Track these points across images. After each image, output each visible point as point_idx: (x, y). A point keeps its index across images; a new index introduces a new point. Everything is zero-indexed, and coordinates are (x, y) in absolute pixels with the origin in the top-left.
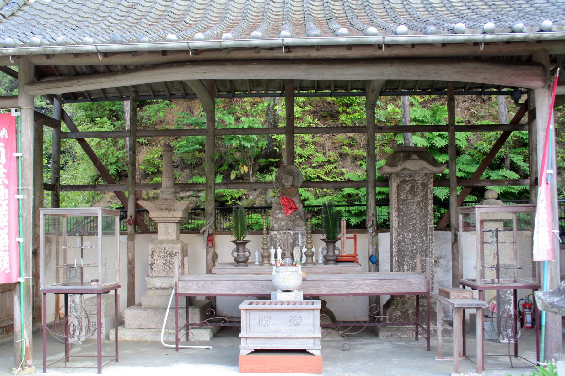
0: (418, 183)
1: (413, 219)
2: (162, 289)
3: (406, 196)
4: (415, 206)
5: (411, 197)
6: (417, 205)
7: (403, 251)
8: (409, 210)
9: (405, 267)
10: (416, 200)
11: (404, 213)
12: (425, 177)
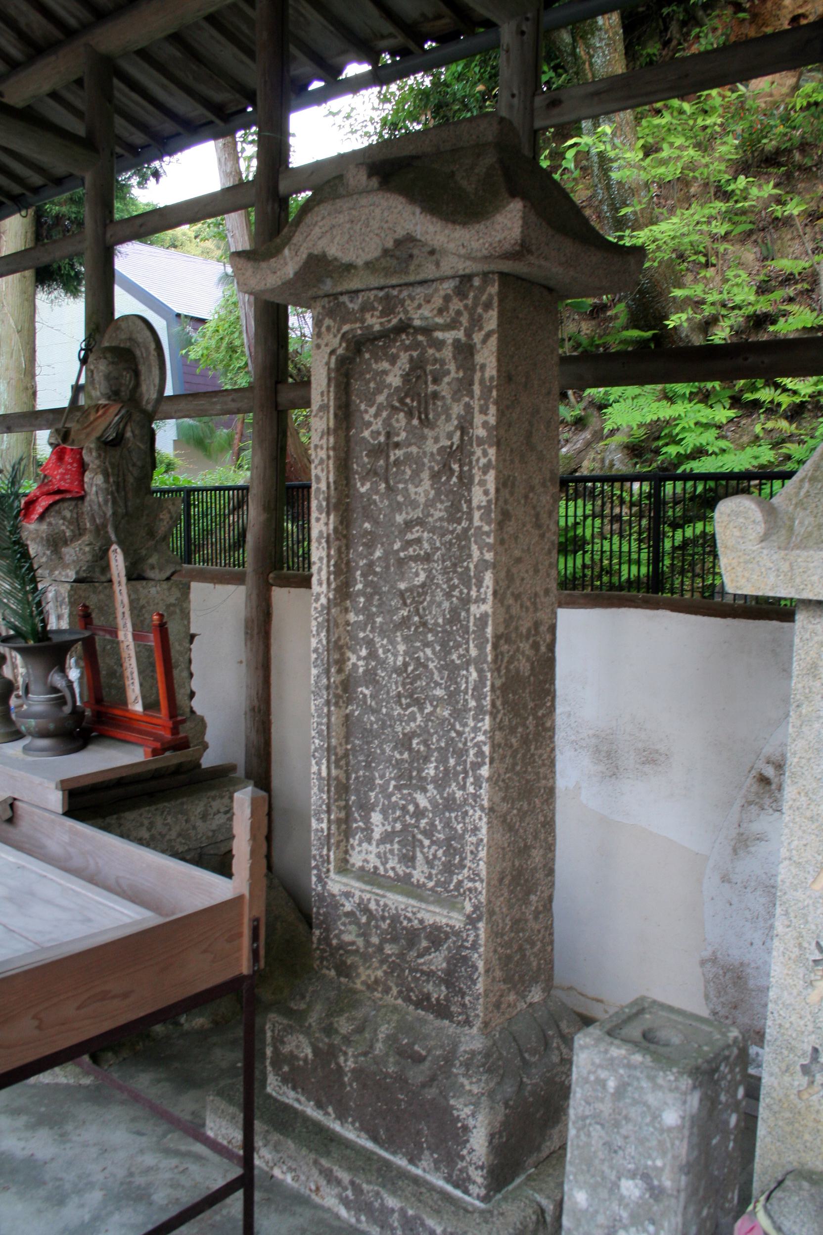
0: (439, 345)
1: (416, 558)
2: (269, 814)
3: (387, 422)
4: (427, 484)
5: (409, 429)
6: (435, 476)
7: (368, 734)
8: (399, 507)
9: (376, 817)
10: (431, 447)
11: (376, 522)
12: (456, 305)
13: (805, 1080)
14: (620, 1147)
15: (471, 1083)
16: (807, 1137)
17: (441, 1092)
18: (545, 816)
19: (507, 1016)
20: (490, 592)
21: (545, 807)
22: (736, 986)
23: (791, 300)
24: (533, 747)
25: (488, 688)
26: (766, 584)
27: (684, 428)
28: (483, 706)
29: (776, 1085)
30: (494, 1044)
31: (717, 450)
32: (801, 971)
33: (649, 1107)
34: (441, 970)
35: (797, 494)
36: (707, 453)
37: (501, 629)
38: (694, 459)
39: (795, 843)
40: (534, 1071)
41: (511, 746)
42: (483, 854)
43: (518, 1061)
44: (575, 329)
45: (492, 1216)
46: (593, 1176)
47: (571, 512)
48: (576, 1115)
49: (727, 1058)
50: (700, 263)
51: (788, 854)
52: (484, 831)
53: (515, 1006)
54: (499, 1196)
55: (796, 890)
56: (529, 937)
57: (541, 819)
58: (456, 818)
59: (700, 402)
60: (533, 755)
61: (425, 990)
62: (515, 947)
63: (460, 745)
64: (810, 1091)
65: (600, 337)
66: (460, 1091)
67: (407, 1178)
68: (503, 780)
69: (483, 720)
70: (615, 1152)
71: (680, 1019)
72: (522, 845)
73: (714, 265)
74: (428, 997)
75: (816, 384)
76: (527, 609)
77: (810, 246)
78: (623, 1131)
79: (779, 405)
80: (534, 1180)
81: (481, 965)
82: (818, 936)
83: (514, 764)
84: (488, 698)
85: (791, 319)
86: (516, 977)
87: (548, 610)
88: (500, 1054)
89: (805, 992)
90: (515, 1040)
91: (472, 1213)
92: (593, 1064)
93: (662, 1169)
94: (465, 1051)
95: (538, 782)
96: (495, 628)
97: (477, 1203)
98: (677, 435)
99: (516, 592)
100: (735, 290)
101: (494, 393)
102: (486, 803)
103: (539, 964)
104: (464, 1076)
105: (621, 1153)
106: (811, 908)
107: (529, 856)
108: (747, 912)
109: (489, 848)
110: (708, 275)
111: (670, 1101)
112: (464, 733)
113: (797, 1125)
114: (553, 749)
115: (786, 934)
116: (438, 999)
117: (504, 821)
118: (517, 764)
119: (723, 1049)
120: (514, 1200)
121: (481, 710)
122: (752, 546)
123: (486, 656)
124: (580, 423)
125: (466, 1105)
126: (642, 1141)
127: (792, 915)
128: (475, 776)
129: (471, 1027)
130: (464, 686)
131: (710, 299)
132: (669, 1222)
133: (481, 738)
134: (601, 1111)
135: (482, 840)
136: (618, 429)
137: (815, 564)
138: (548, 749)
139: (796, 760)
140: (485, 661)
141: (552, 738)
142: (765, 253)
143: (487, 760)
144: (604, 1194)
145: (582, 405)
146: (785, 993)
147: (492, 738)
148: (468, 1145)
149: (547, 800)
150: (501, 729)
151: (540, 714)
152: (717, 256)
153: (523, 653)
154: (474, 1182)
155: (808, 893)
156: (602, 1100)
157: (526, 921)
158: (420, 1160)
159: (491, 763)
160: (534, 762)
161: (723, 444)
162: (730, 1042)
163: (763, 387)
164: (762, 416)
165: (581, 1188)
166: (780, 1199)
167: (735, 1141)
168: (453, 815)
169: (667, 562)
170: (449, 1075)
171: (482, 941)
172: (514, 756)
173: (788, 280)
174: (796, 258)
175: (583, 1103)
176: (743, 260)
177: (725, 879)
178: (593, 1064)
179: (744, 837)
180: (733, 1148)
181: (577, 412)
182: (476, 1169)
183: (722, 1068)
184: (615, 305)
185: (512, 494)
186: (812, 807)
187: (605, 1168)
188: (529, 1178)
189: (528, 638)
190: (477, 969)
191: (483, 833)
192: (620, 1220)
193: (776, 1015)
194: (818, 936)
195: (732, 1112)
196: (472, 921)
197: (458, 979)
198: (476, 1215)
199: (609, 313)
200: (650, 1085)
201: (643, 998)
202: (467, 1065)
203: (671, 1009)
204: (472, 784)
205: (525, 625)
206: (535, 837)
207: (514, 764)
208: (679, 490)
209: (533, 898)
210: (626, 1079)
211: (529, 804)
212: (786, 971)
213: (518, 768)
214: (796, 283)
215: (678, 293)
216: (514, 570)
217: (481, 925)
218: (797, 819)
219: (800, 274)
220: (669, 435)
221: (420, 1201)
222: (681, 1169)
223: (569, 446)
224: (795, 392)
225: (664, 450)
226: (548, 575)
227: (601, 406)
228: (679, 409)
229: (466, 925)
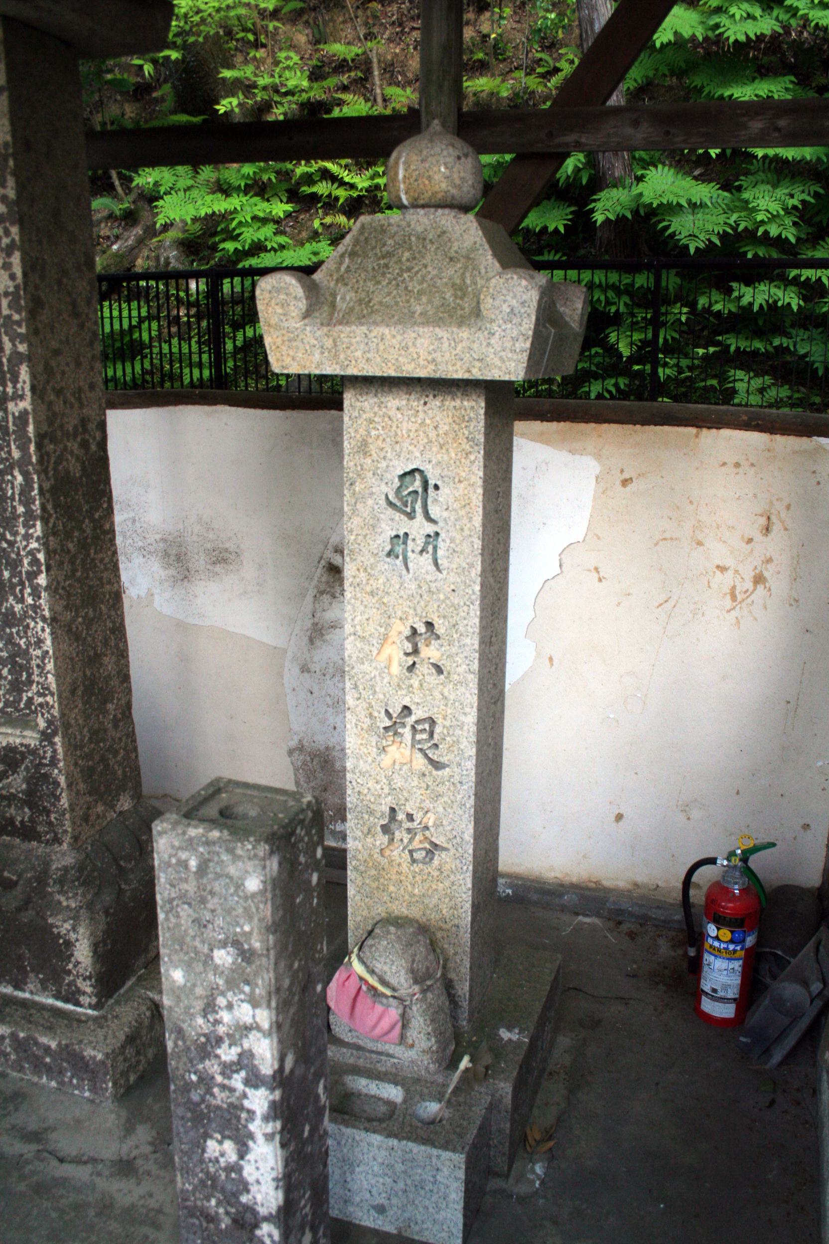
13: (386, 839)
14: (208, 921)
15: (68, 899)
16: (392, 888)
17: (38, 913)
18: (114, 622)
19: (97, 828)
20: (27, 387)
21: (113, 613)
22: (323, 767)
23: (345, 88)
24: (92, 551)
25: (36, 492)
26: (312, 362)
27: (240, 223)
28: (33, 511)
29: (360, 847)
30: (87, 856)
31: (276, 246)
32: (374, 740)
33: (231, 878)
34: (22, 792)
35: (338, 269)
36: (266, 250)
37: (45, 428)
38: (253, 255)
39: (358, 618)
40: (131, 877)
41: (69, 551)
42: (50, 666)
43: (113, 870)
44: (118, 112)
45: (106, 1020)
46: (187, 953)
47: (125, 313)
48: (162, 899)
49: (302, 822)
50: (249, 41)
51: (352, 630)
52: (49, 642)
53: (104, 816)
54: (111, 1001)
55: (363, 663)
56: (111, 746)
57: (109, 624)
58: (18, 633)
59: (256, 195)
60: (93, 560)
61: (8, 815)
62: (97, 758)
63: (13, 556)
64: (391, 847)
65: (146, 121)
66: (57, 908)
67: (14, 1004)
68: (64, 588)
69: (34, 526)
70: (205, 926)
71: (255, 793)
72: (92, 653)
73: (264, 46)
74: (12, 821)
75: (372, 178)
76: (72, 406)
77: (362, 32)
78: (210, 906)
79: (337, 199)
80: (145, 980)
81: (62, 780)
82: (386, 705)
83: (74, 571)
84: (37, 502)
85: (345, 109)
86: (102, 788)
87: (95, 406)
88: (94, 865)
89: (379, 758)
90: (108, 849)
91: (86, 1022)
92: (173, 847)
93: (250, 933)
94: (57, 869)
95: (102, 587)
96: (36, 428)
97: (90, 1012)
98: (234, 229)
99: (58, 387)
100: (287, 74)
101: (11, 163)
102: (47, 613)
103: (124, 772)
104: (59, 892)
105: (210, 926)
106: (378, 678)
107: (101, 664)
108: (328, 698)
109: (56, 659)
110: (258, 55)
111: (250, 869)
112: (16, 542)
113: (382, 880)
114: (115, 553)
115: (357, 706)
116: (22, 822)
117: (70, 630)
118: (77, 570)
119: (297, 814)
120: (126, 1001)
121: (31, 516)
122: (295, 323)
123: (30, 457)
124: (129, 218)
125: (65, 921)
126: (229, 911)
127: (361, 687)
128: (31, 586)
129: (60, 844)
130: (10, 493)
131: (261, 82)
132: (263, 979)
133: (34, 545)
134: (187, 891)
135: (47, 652)
136: (172, 224)
137: (358, 339)
138: (109, 553)
139: (353, 537)
140: (31, 463)
141: (113, 540)
142: (317, 36)
143: (43, 568)
144: (199, 967)
145: (131, 198)
146: (361, 762)
147: (46, 545)
148: (73, 959)
149: (114, 606)
150: (55, 534)
151: (97, 516)
152: (267, 36)
153: (72, 453)
154: (84, 993)
155: (374, 665)
156: (186, 880)
157: (105, 730)
158: (26, 984)
159: (48, 570)
160: (95, 566)
161: (282, 239)
162: (304, 806)
163: (321, 180)
164: (320, 211)
165: (176, 967)
166: (371, 946)
167: (318, 897)
168: (14, 630)
169: (230, 364)
170: (43, 895)
171: (60, 756)
172: (72, 562)
173: (342, 66)
174: (349, 43)
175: (168, 886)
176: (295, 42)
177: (305, 669)
178: (173, 847)
179: (319, 626)
180: (318, 904)
181: (126, 205)
182: (84, 980)
183: (298, 831)
184: (160, 87)
185: (42, 277)
186: (371, 582)
187: (197, 943)
188: (140, 979)
189: (75, 436)
190: (59, 784)
191: (48, 643)
192: (218, 988)
193: (354, 783)
194: (386, 705)
195: (313, 871)
196: (47, 737)
197: (40, 798)
198: (90, 1023)
199: (155, 95)
200: (230, 857)
201: (219, 779)
202: (61, 881)
203: (247, 785)
204: (30, 595)
205: (71, 423)
206: (106, 643)
207: (74, 571)
208: (238, 289)
209: (110, 706)
210: (207, 856)
211: (95, 610)
212: (360, 742)
213: (79, 574)
214: (350, 70)
215: (227, 74)
216: (53, 363)
217: (57, 739)
218: (359, 595)
219: (353, 60)
220: (226, 230)
221: (30, 1022)
222: (268, 929)
223: (119, 242)
224: (352, 186)
225: (222, 246)
226: (92, 368)
227: (151, 198)
228: (235, 202)
229: (41, 742)
